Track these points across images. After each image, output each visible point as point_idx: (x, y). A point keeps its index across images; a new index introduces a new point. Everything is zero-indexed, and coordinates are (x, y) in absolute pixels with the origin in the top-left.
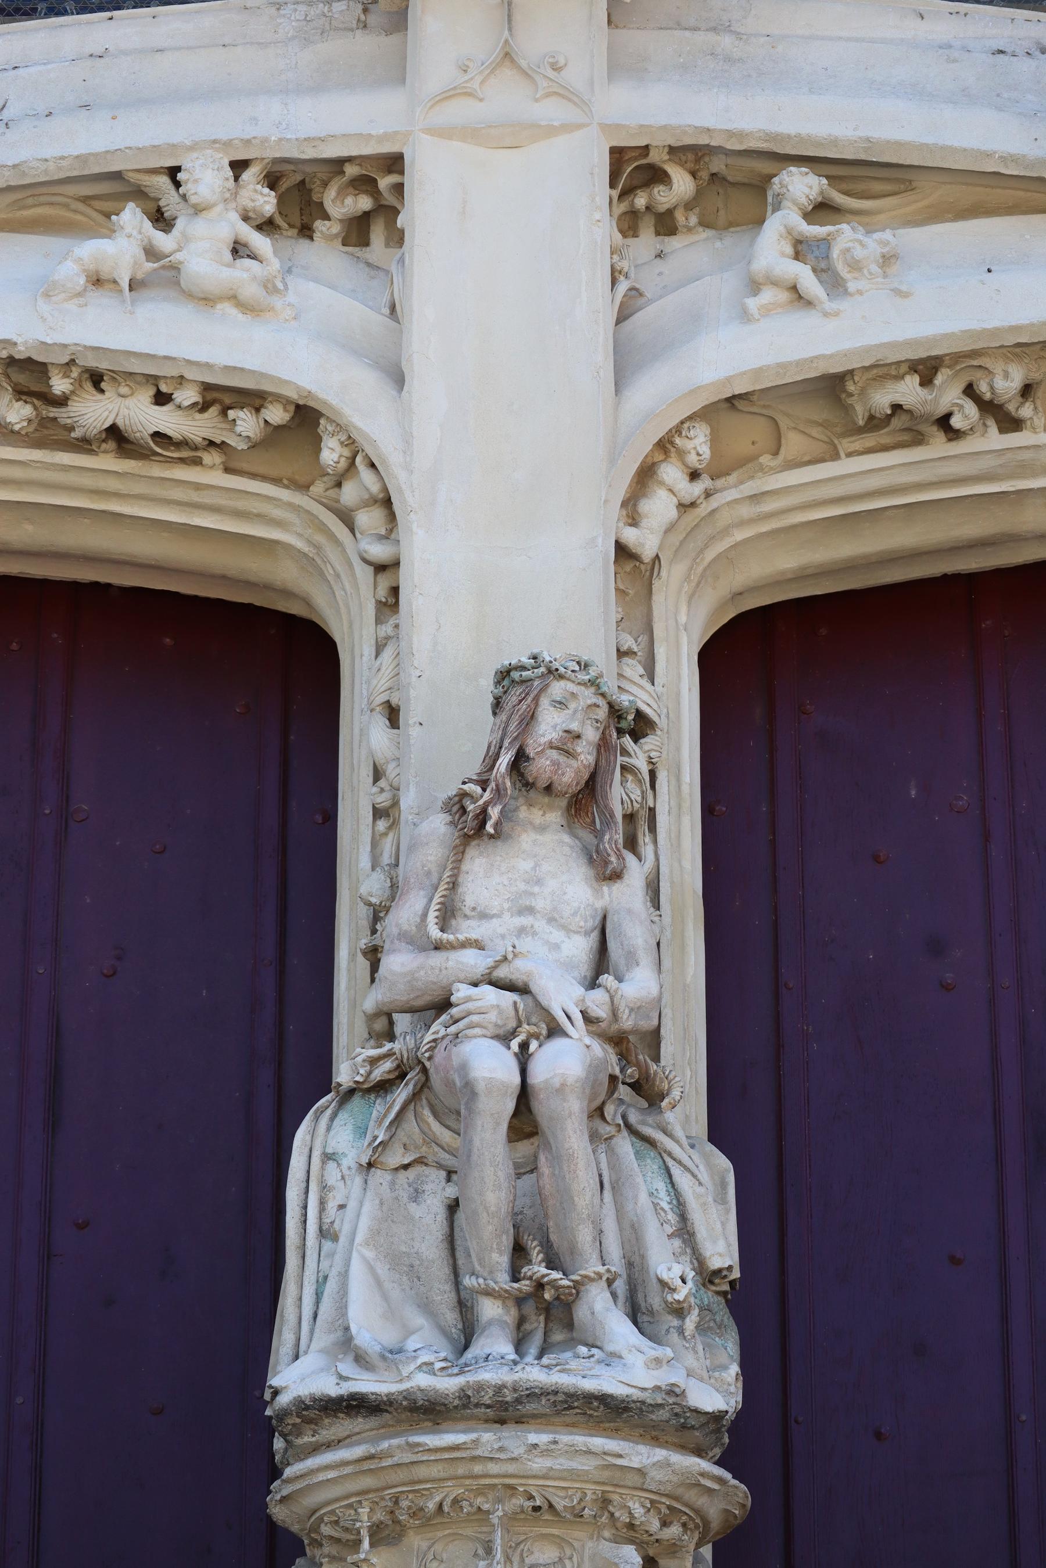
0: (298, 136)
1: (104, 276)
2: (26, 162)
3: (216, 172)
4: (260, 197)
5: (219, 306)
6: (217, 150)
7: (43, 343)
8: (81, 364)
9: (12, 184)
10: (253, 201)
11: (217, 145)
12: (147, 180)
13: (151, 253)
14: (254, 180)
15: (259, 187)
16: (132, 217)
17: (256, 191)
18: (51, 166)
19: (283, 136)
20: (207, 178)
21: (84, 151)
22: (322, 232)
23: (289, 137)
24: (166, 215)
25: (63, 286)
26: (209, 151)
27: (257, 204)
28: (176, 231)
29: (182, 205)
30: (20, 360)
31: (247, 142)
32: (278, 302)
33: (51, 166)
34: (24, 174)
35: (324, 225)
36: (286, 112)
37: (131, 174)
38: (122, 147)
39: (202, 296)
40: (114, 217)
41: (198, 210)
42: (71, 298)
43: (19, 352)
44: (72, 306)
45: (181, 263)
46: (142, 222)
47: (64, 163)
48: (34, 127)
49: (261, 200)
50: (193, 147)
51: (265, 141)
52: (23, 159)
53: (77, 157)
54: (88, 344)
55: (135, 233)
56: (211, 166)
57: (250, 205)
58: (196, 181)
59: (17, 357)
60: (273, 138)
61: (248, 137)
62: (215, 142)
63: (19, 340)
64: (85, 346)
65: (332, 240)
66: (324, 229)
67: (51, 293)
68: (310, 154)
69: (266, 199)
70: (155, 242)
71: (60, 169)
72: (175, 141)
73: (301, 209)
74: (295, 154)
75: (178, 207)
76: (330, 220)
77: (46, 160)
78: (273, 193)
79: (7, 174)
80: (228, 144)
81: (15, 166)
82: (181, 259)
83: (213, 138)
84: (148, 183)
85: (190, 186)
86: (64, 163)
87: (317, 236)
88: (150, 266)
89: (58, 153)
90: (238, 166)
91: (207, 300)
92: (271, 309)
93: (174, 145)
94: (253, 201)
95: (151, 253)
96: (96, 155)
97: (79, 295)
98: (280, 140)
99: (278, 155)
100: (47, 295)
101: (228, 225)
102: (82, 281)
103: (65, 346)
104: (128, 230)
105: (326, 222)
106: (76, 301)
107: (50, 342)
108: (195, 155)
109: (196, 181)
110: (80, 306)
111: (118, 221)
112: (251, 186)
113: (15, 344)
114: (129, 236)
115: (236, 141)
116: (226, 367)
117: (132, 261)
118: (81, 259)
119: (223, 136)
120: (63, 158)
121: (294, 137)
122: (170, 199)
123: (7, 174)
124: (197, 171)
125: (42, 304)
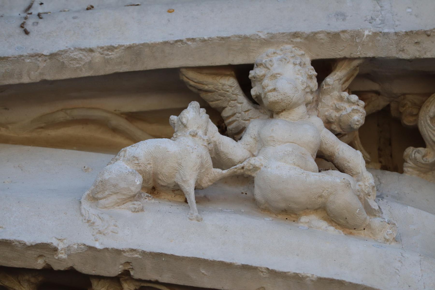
0: (398, 30)
1: (164, 181)
2: (66, 51)
3: (298, 67)
4: (346, 105)
5: (304, 219)
6: (298, 46)
7: (91, 248)
8: (137, 276)
9: (48, 78)
10: (337, 109)
11: (298, 40)
12: (210, 82)
13: (219, 160)
14: (337, 85)
15: (346, 94)
16: (193, 115)
17: (341, 99)
18: (97, 57)
19: (378, 30)
20: (286, 75)
21: (137, 42)
22: (415, 160)
23: (386, 30)
24: (230, 127)
25: (115, 186)
26: (289, 47)
27: (344, 113)
28: (247, 138)
29: (253, 112)
30: (59, 271)
31: (335, 37)
32: (376, 222)
33: (97, 57)
34: (63, 66)
35: (418, 152)
36: (378, 8)
37: (191, 74)
38: (184, 38)
39: (282, 205)
40: (173, 118)
41: (273, 112)
42: (124, 201)
43: (60, 260)
44: (125, 211)
45: (256, 169)
46: (208, 122)
47: (113, 55)
48: (74, 18)
49: (348, 108)
50: (271, 40)
51: (356, 35)
52: (62, 48)
53: (130, 48)
54: (148, 249)
55: (200, 133)
56: (292, 60)
57: (335, 114)
58: (274, 77)
59: (56, 267)
60: (366, 33)
61: (336, 30)
62: (295, 35)
63: (61, 246)
64: (144, 253)
65: (425, 173)
66: (418, 156)
67: (99, 196)
68: (411, 52)
69: (355, 107)
70: (222, 148)
71: (107, 62)
72: (248, 32)
73: (379, 149)
74: (393, 52)
75: (246, 115)
76: (424, 146)
77: (91, 50)
78: (362, 103)
79: (42, 65)
80: (311, 39)
81: (52, 56)
82: (257, 164)
83: (294, 30)
84: (211, 87)
85: (266, 82)
86: (113, 55)
87: (409, 166)
88: (218, 172)
89: (105, 42)
90: (323, 68)
91: (287, 211)
92: (367, 227)
93: (246, 38)
94: (337, 109)
95: (219, 160)
96: (152, 46)
97: (134, 197)
98: (375, 34)
99: (370, 54)
100: (94, 199)
101: (310, 130)
102: (138, 181)
103: (118, 252)
104: (192, 128)
105: (421, 149)
106: (130, 205)
107: (98, 246)
108: (271, 50)
109: (274, 77)
110: (136, 211)
111: (180, 120)
112: (336, 93)
113: (55, 250)
114: (194, 135)
115: (322, 36)
116: (320, 280)
117: (199, 161)
118: (137, 159)
119: (305, 28)
120: (111, 48)
121: (392, 31)
122: (237, 105)
123: (42, 65)
124: (275, 65)
125: (87, 207)
